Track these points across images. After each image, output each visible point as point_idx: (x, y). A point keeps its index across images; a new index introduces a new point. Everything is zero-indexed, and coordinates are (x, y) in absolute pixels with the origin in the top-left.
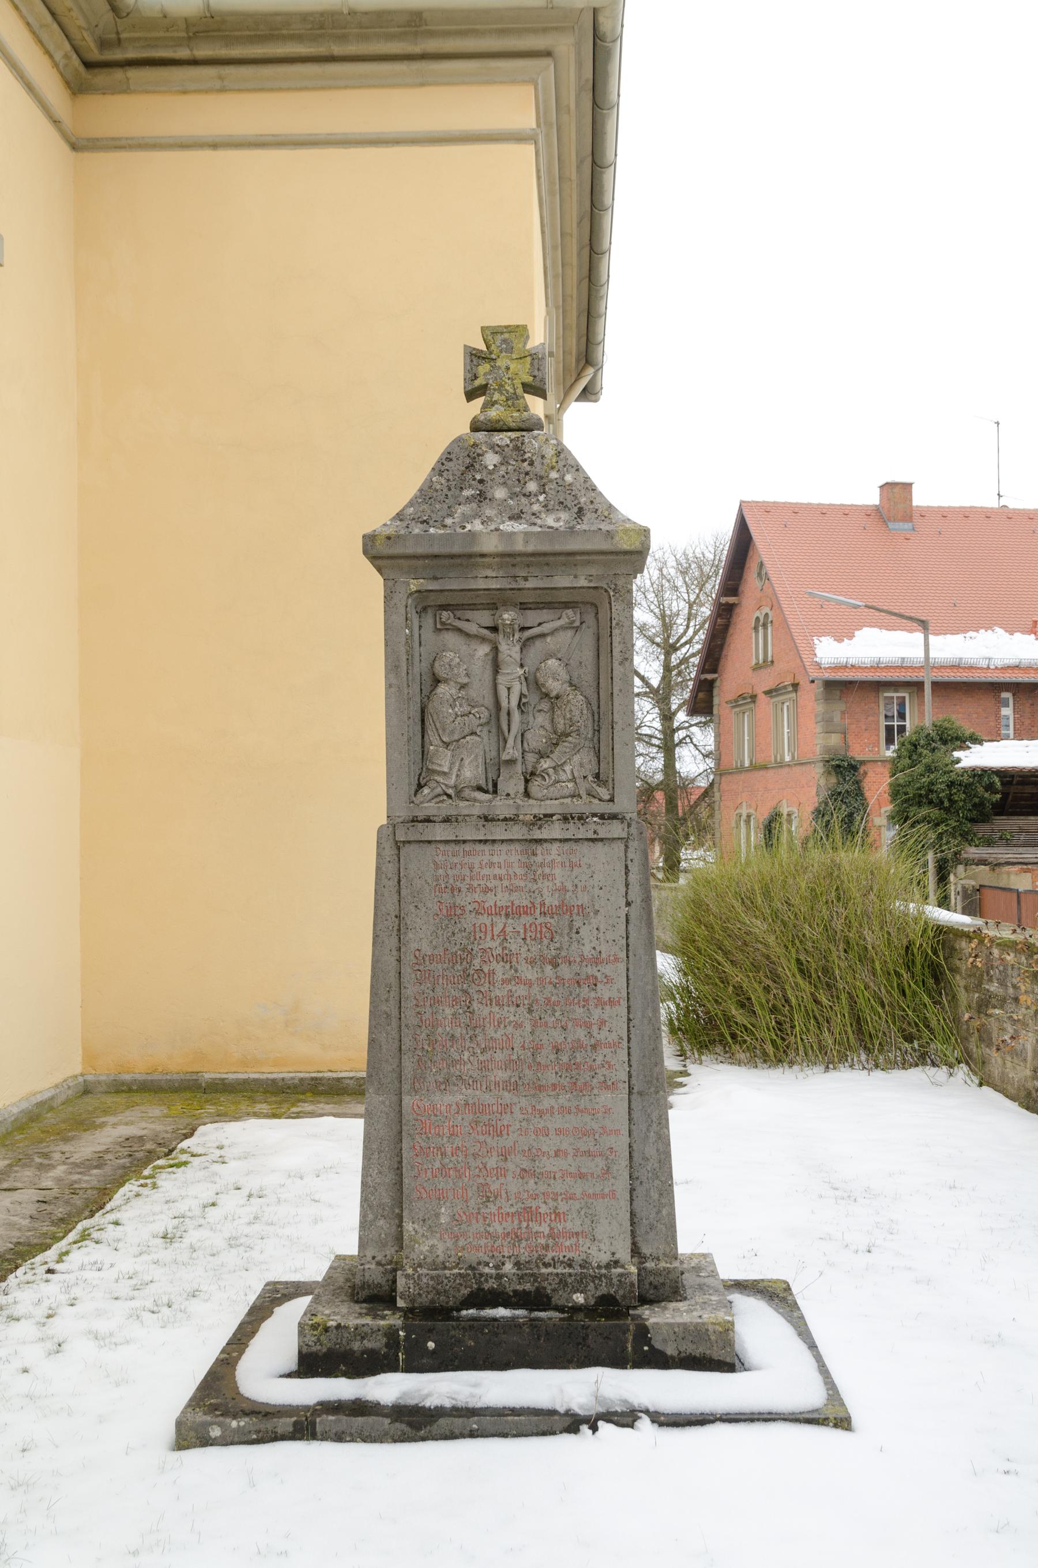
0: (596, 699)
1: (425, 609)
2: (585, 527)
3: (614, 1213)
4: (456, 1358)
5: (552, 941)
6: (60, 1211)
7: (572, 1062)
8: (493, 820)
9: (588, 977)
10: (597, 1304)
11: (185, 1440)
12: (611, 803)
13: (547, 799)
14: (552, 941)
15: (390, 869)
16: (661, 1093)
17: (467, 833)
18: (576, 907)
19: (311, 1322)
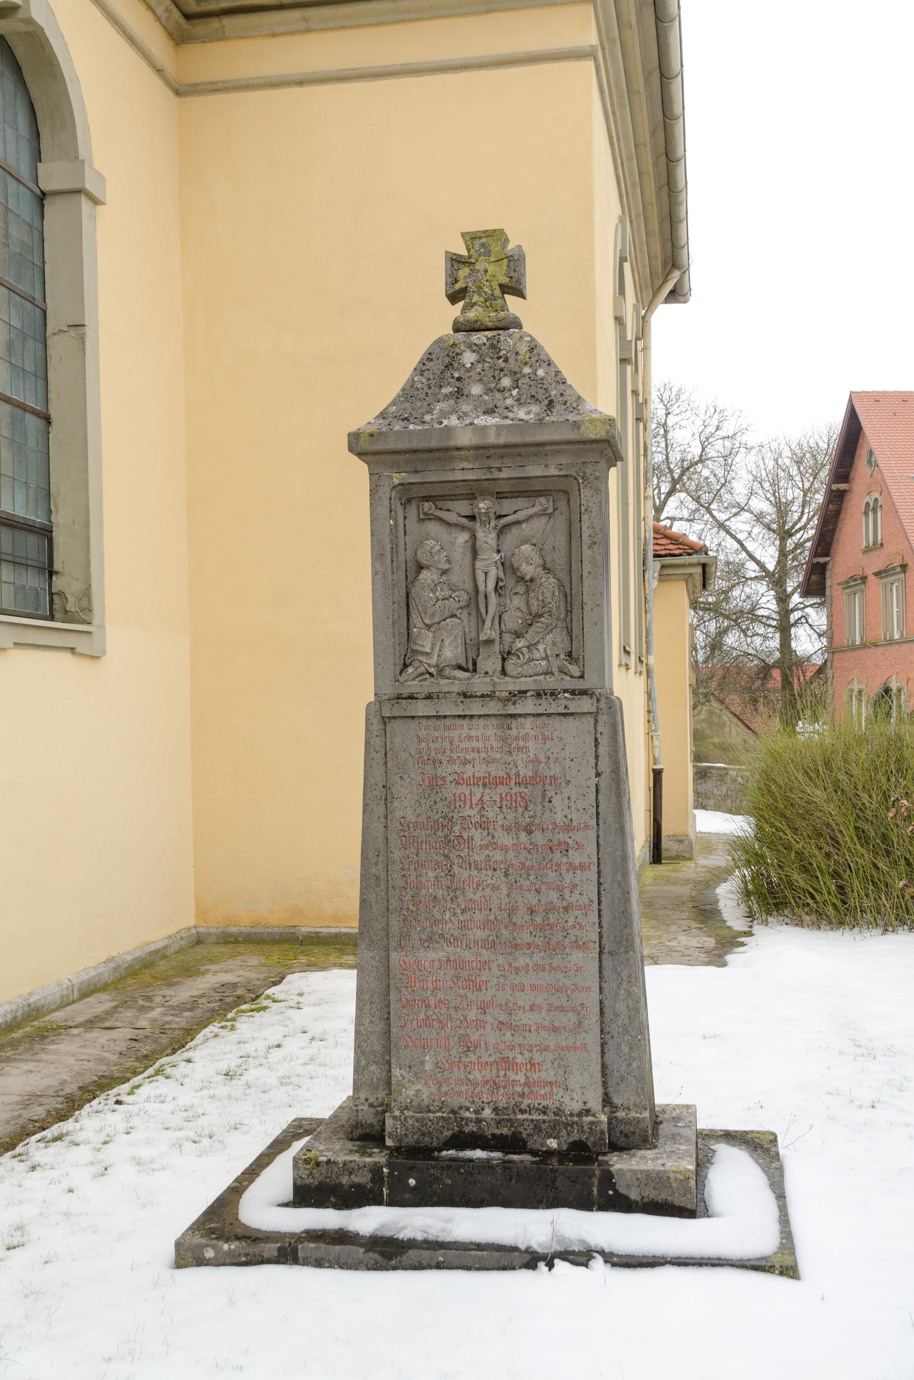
0: (568, 582)
1: (409, 501)
2: (553, 418)
3: (586, 1065)
4: (435, 1195)
5: (526, 809)
6: (146, 1049)
7: (546, 923)
8: (471, 696)
9: (560, 844)
10: (569, 1149)
11: (183, 1259)
12: (581, 680)
13: (522, 676)
14: (526, 809)
15: (378, 742)
16: (631, 953)
17: (447, 709)
18: (548, 778)
19: (304, 1157)
